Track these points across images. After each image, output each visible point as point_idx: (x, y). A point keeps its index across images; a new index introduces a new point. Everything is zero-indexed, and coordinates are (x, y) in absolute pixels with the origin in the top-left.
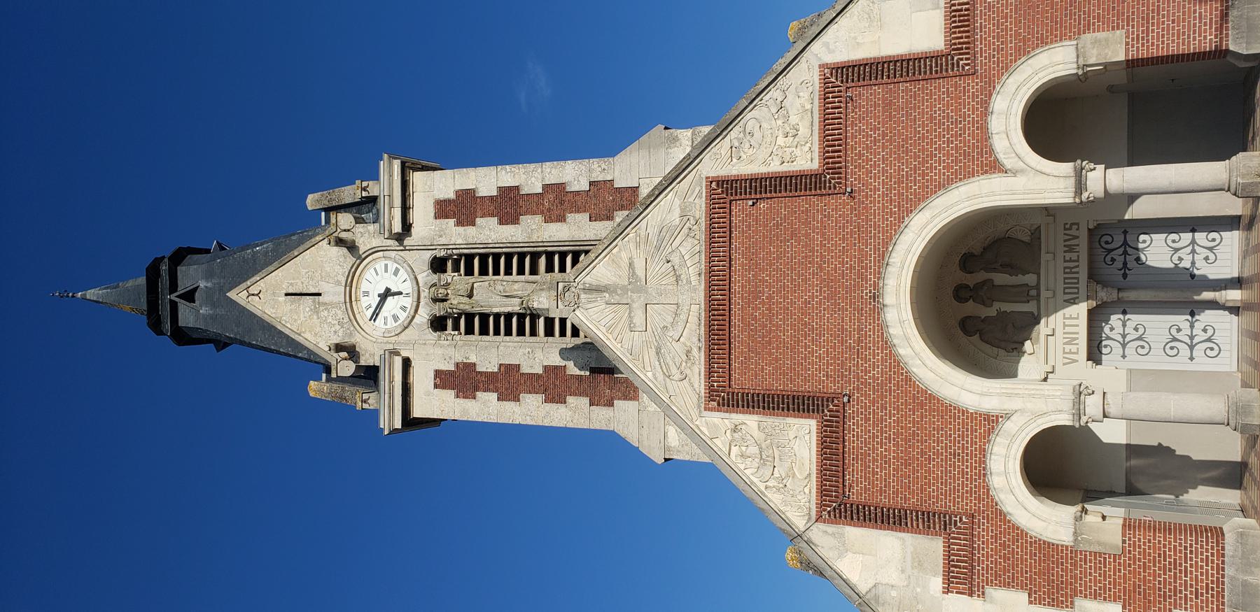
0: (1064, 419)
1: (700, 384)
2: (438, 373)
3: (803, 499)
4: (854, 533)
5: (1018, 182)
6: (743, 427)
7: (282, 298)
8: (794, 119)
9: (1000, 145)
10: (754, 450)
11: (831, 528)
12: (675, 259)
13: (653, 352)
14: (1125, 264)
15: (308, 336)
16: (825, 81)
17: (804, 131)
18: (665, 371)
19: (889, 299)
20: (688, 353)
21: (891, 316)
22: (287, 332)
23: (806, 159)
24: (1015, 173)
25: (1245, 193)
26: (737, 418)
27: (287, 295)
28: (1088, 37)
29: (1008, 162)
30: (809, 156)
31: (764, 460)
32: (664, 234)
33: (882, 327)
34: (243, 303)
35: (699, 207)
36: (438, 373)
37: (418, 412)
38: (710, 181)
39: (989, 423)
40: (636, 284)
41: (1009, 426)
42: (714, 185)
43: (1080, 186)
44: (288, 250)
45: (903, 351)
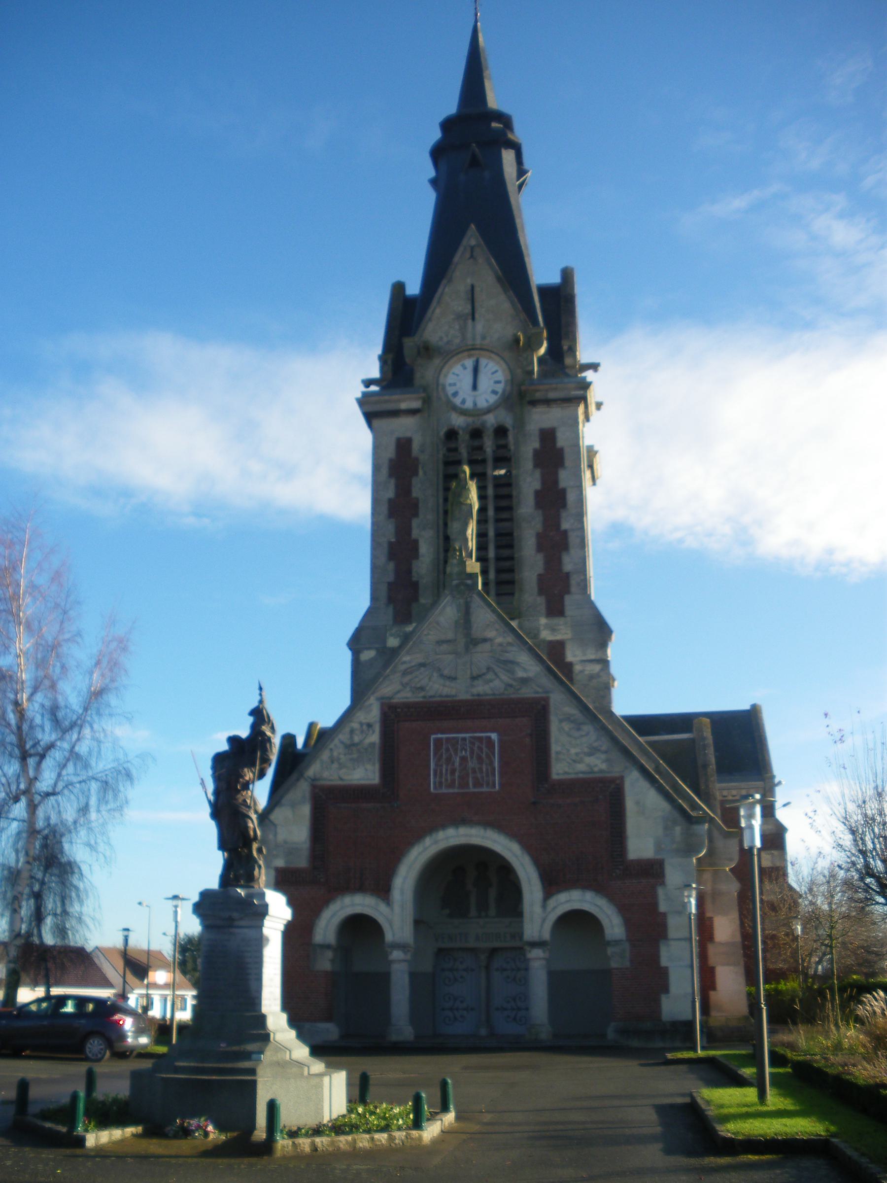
0: (389, 937)
1: (398, 699)
2: (409, 441)
3: (326, 774)
4: (306, 810)
5: (538, 909)
6: (371, 732)
7: (469, 281)
8: (588, 760)
9: (563, 897)
10: (356, 739)
11: (308, 795)
12: (490, 676)
13: (421, 660)
14: (505, 1009)
15: (438, 311)
16: (612, 780)
17: (581, 767)
18: (408, 670)
19: (463, 830)
20: (422, 689)
21: (451, 831)
22: (440, 290)
23: (559, 770)
24: (544, 906)
25: (355, 725)
26: (377, 728)
27: (473, 287)
28: (627, 946)
29: (552, 902)
30: (561, 771)
31: (350, 747)
32: (509, 665)
33: (444, 827)
34: (465, 242)
35: (527, 692)
36: (409, 441)
37: (311, 1073)
38: (546, 700)
39: (383, 890)
40: (473, 642)
41: (383, 907)
42: (543, 703)
43: (534, 945)
44: (367, 655)
45: (428, 841)
